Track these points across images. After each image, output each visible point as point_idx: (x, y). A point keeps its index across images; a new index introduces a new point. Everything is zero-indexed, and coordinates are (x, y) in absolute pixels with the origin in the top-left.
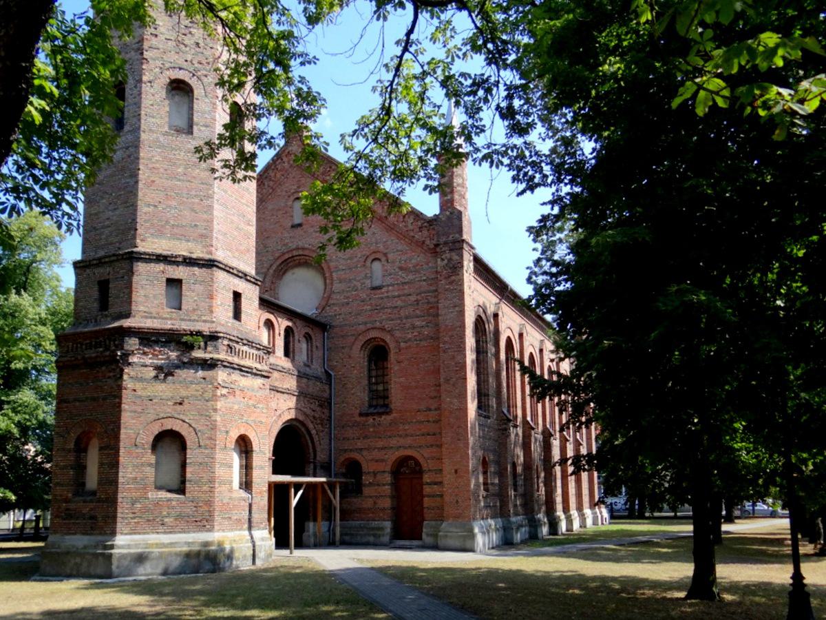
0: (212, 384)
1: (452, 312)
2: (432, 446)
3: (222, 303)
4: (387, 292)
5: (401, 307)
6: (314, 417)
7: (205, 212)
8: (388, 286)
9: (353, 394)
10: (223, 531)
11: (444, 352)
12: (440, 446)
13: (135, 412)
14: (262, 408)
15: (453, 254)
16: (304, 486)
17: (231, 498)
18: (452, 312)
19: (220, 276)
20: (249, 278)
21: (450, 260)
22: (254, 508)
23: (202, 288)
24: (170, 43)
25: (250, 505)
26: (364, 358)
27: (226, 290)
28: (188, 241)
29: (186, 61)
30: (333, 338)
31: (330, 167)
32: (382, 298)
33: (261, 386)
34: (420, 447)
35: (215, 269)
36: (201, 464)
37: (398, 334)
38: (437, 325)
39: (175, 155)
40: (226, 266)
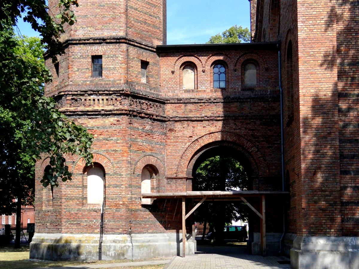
3: (78, 69)
10: (72, 233)
16: (203, 200)
20: (108, 41)
22: (105, 216)
25: (102, 215)
33: (115, 122)
35: (70, 46)
40: (80, 40)
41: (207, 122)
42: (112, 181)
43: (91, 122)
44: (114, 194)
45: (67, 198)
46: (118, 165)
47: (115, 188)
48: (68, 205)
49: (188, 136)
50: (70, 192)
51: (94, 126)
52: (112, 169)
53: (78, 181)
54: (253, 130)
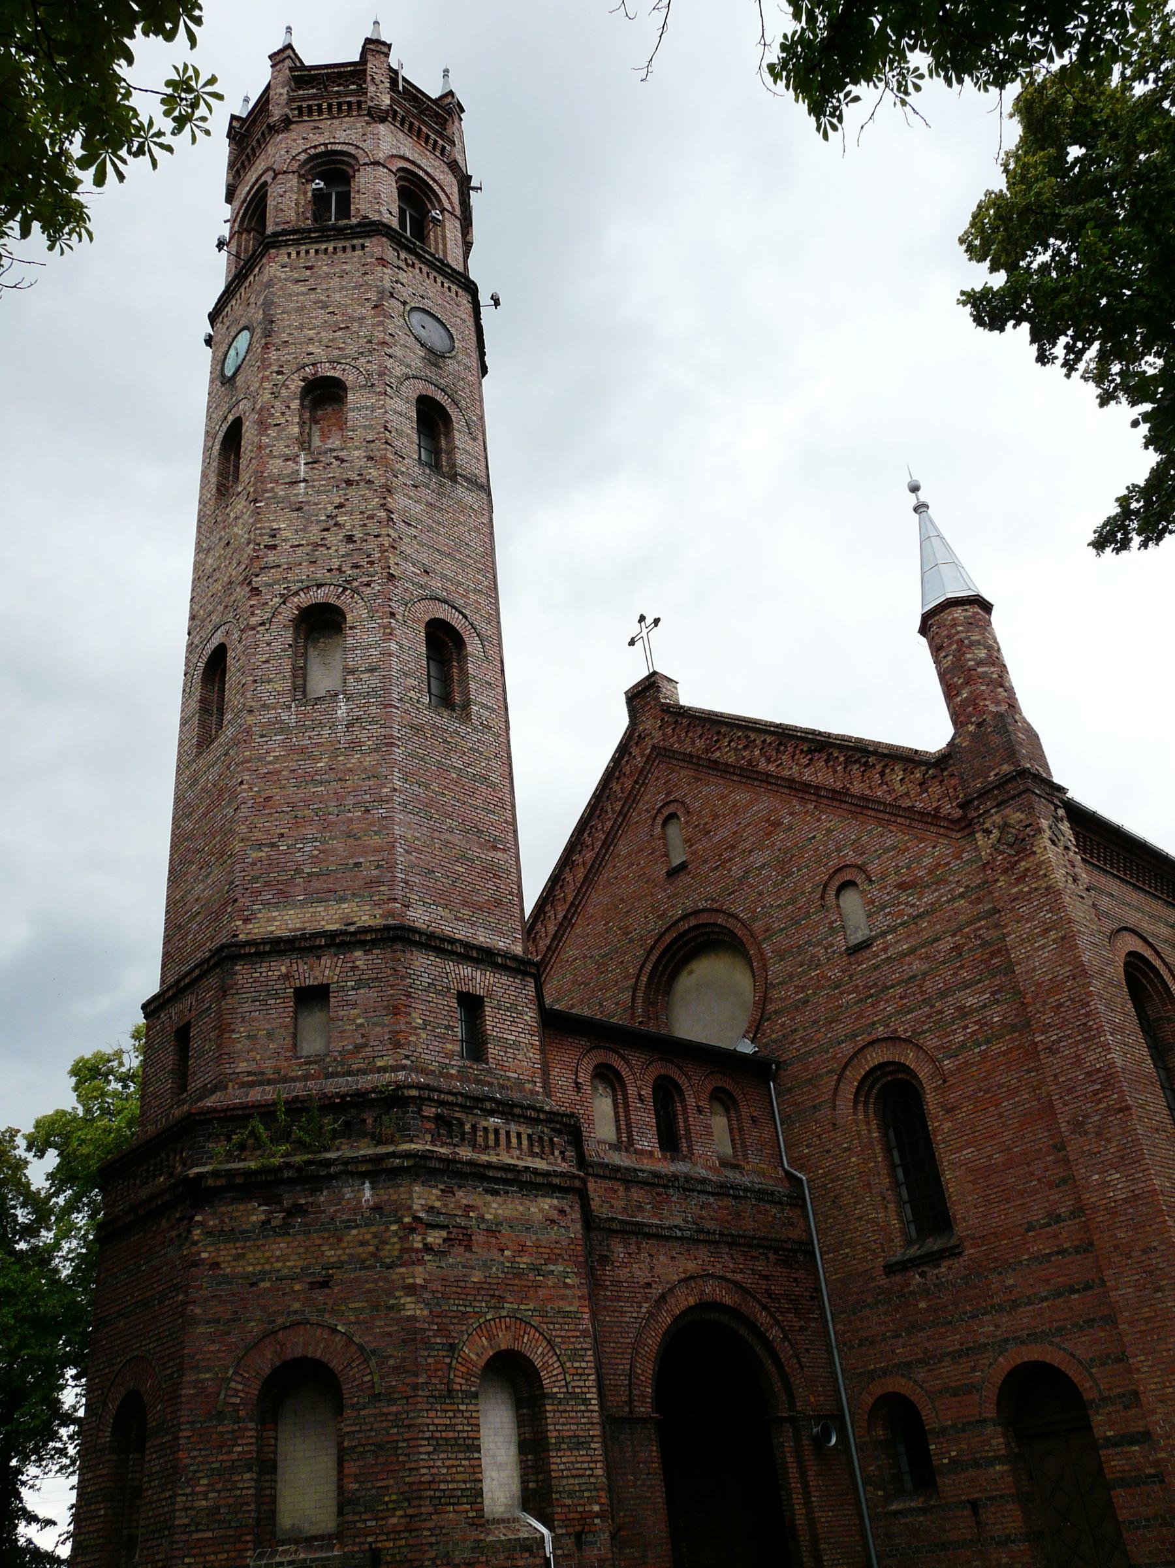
0: (399, 1221)
1: (1043, 947)
2: (1090, 1322)
3: (426, 1023)
4: (885, 950)
5: (925, 974)
6: (769, 1294)
7: (376, 833)
8: (884, 934)
9: (860, 1218)
11: (1052, 1051)
12: (1111, 1320)
13: (217, 1321)
14: (566, 1275)
15: (1008, 811)
17: (478, 1547)
18: (1043, 947)
19: (422, 963)
21: (1004, 827)
23: (373, 994)
24: (299, 550)
26: (868, 1123)
27: (438, 993)
28: (342, 900)
29: (330, 570)
30: (789, 1090)
31: (719, 733)
32: (876, 967)
33: (554, 1214)
34: (1059, 1329)
36: (380, 1447)
37: (930, 1041)
38: (1018, 992)
39: (310, 738)
41: (677, 1244)
42: (563, 1424)
43: (494, 1205)
44: (574, 1472)
45: (438, 1494)
46: (576, 1364)
47: (575, 1453)
48: (442, 1528)
49: (642, 1281)
50: (444, 1471)
51: (501, 1219)
52: (560, 1377)
53: (469, 1425)
54: (766, 1277)
